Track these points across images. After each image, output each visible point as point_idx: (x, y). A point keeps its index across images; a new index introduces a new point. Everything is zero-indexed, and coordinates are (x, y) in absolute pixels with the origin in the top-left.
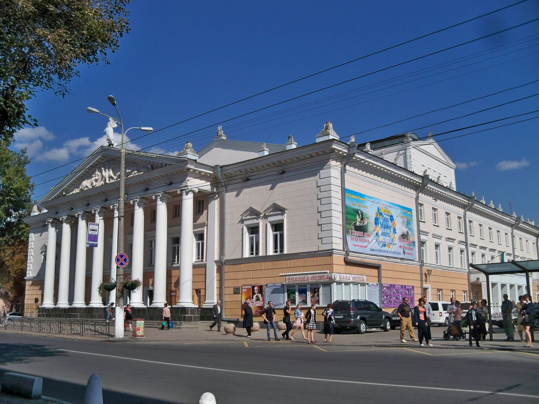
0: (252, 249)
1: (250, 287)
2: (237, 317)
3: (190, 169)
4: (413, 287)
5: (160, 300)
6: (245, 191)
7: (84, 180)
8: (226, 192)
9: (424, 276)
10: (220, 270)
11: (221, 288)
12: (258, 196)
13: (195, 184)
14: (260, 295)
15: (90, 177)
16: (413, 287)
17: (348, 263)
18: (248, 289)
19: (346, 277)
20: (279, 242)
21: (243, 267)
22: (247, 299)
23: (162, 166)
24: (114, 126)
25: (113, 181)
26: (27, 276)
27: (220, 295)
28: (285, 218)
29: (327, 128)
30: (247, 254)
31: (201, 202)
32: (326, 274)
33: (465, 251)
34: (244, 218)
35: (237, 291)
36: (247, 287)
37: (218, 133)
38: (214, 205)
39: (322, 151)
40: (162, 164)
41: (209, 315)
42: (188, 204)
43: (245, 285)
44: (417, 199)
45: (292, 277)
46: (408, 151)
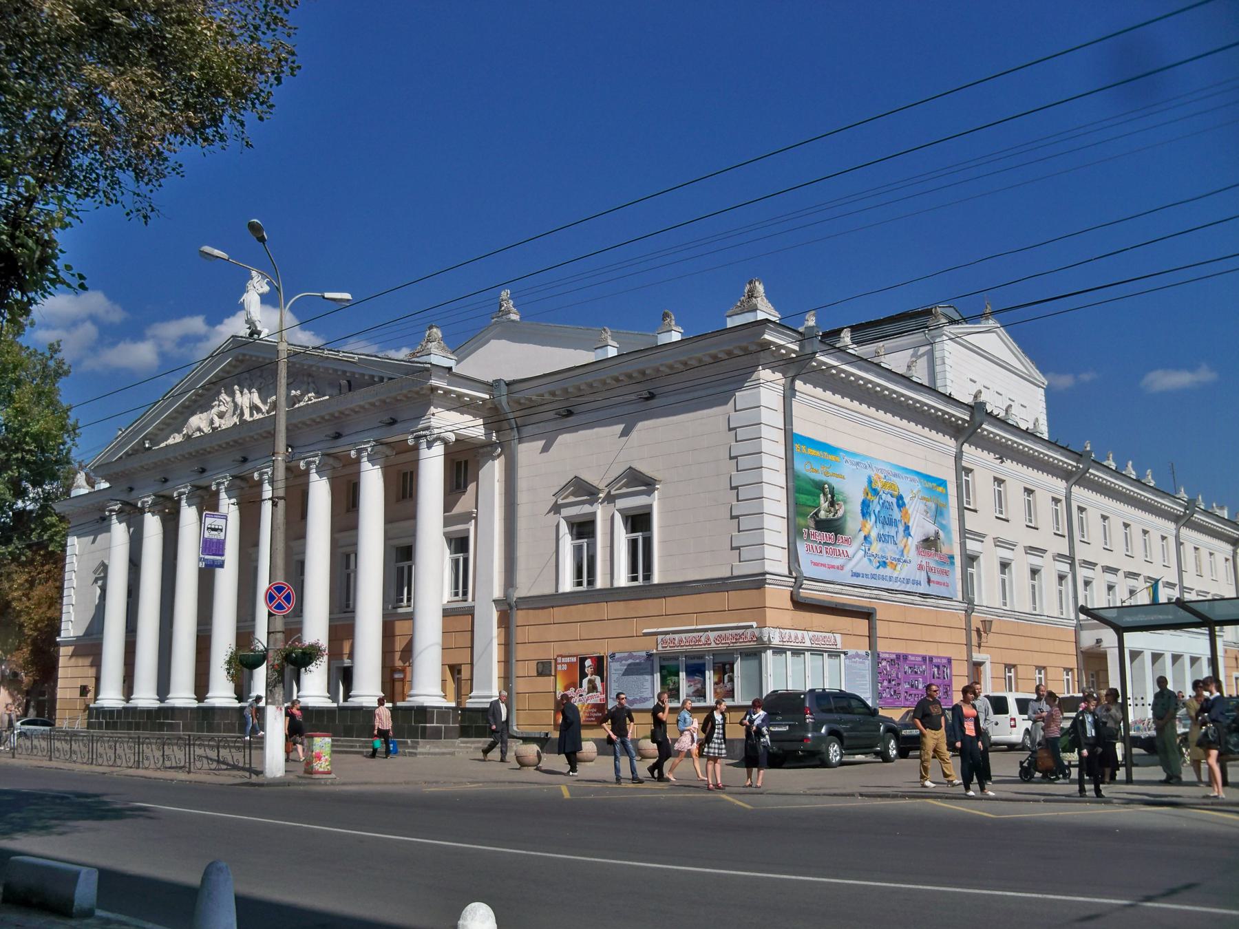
0: (579, 573)
1: (574, 659)
2: (545, 729)
3: (438, 388)
4: (949, 660)
5: (368, 689)
6: (564, 438)
7: (193, 414)
8: (521, 440)
9: (974, 634)
10: (505, 621)
11: (507, 662)
12: (592, 451)
13: (448, 422)
14: (598, 679)
15: (206, 407)
16: (949, 660)
17: (800, 604)
18: (570, 664)
19: (796, 637)
20: (641, 557)
21: (558, 613)
22: (567, 688)
23: (372, 382)
24: (261, 291)
25: (260, 416)
26: (63, 634)
27: (507, 679)
28: (656, 502)
29: (751, 295)
30: (567, 584)
31: (462, 465)
32: (749, 631)
33: (1070, 577)
34: (560, 502)
35: (544, 669)
36: (568, 660)
37: (501, 306)
38: (493, 472)
39: (741, 348)
40: (372, 377)
41: (481, 724)
42: (432, 469)
43: (562, 656)
44: (959, 457)
45: (671, 636)
46: (937, 347)
